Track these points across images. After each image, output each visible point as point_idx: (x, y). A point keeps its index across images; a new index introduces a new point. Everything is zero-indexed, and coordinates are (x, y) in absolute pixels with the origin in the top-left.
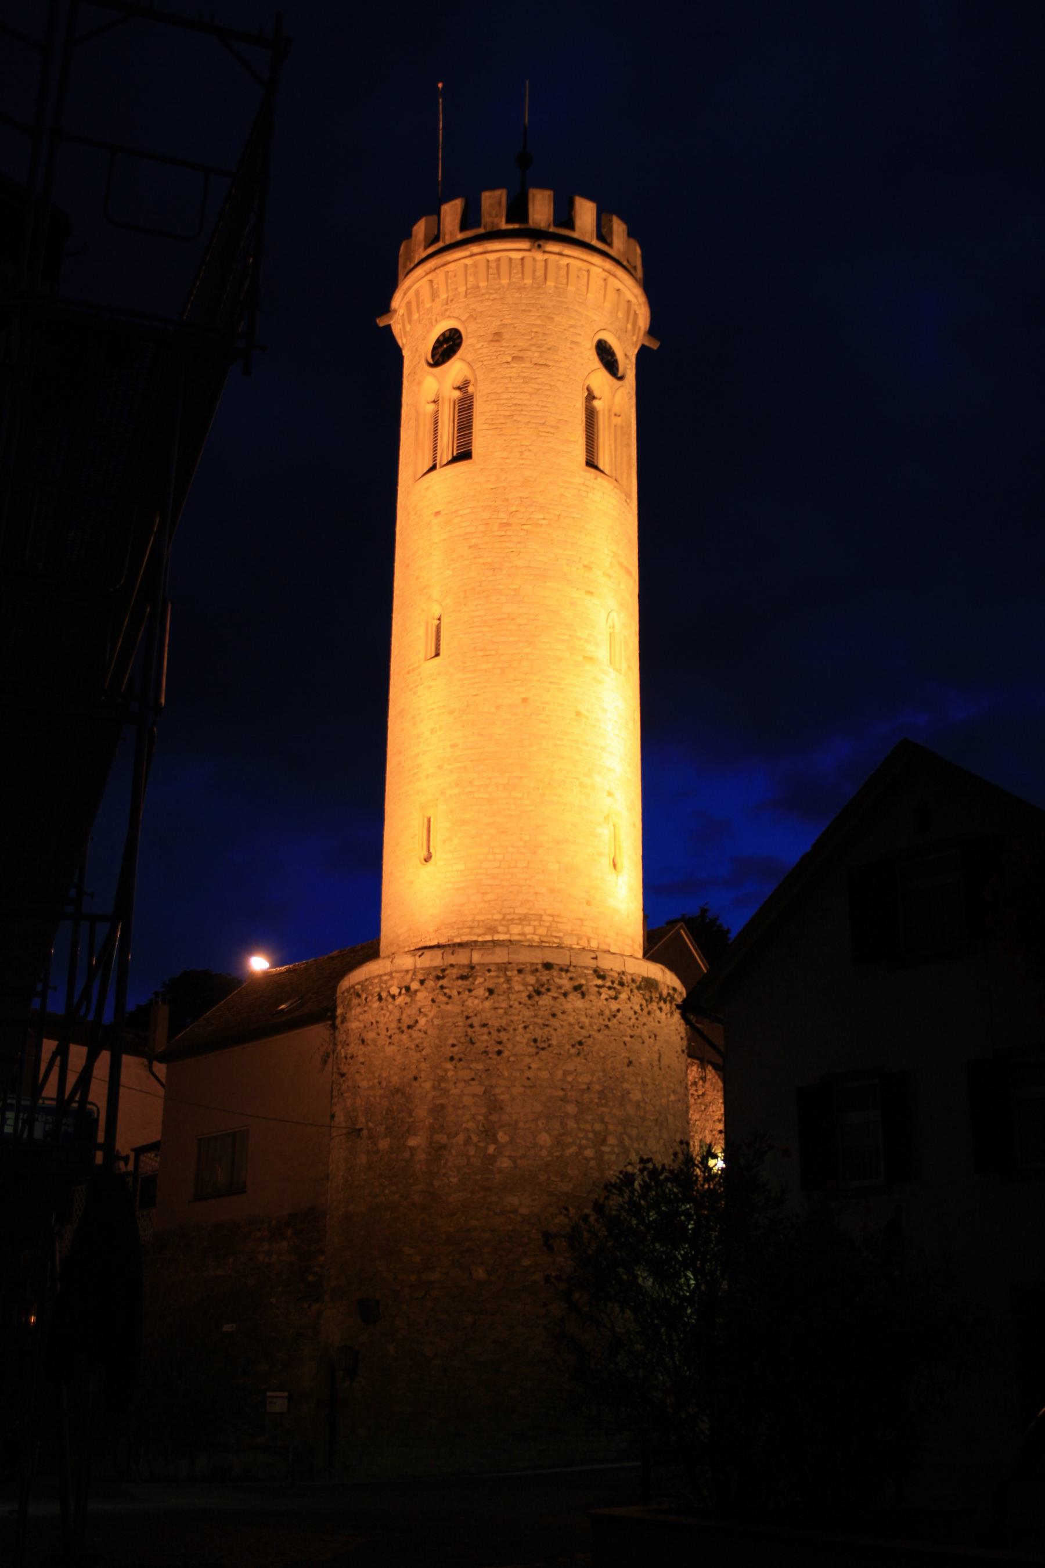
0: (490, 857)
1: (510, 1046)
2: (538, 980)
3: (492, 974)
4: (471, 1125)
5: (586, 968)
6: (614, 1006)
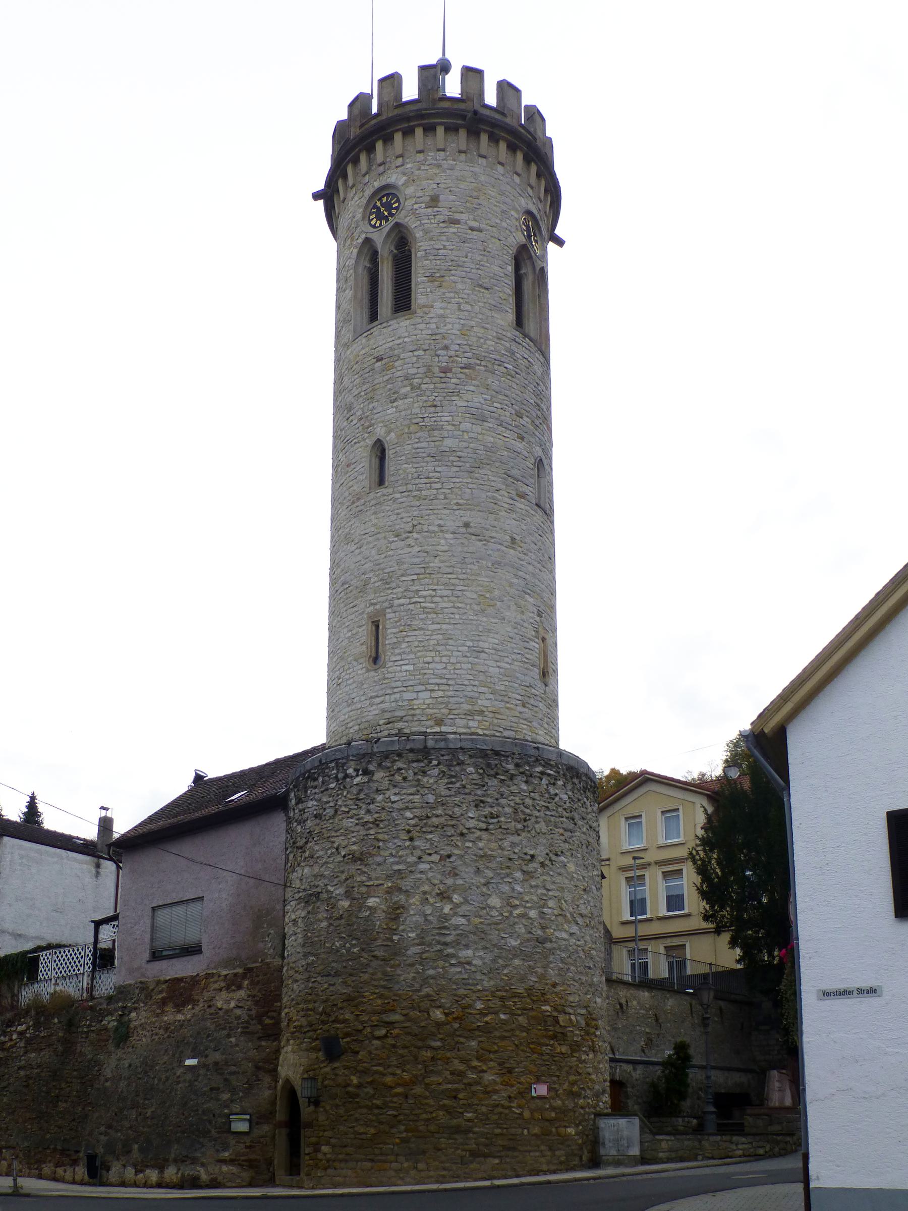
3: (445, 758)
5: (530, 756)
6: (552, 790)
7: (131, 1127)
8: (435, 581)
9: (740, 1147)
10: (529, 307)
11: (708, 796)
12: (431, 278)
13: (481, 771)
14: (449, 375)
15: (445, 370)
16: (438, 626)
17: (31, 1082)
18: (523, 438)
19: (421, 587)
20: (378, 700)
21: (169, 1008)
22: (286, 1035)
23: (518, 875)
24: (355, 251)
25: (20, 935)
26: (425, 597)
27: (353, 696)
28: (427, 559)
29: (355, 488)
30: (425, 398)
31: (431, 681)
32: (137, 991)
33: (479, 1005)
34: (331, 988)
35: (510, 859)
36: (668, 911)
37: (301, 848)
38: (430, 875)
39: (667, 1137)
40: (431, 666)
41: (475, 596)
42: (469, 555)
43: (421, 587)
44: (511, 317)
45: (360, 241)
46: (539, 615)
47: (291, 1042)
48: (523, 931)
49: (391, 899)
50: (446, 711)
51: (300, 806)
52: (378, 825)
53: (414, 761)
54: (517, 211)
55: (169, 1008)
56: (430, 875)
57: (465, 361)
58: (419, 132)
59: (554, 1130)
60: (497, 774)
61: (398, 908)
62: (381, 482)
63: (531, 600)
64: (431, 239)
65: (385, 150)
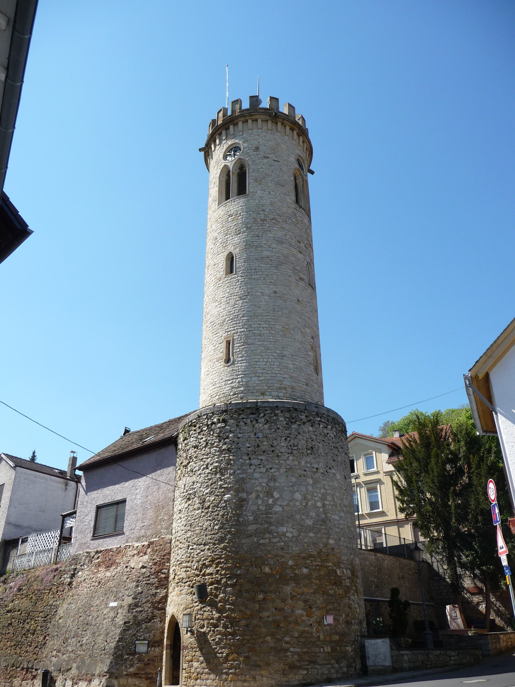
0: (261, 360)
1: (278, 447)
2: (291, 416)
3: (268, 412)
4: (259, 488)
5: (313, 412)
6: (326, 431)
7: (72, 651)
8: (260, 320)
9: (452, 658)
10: (300, 195)
11: (388, 445)
12: (256, 180)
13: (288, 419)
14: (265, 223)
15: (263, 220)
16: (262, 343)
17: (13, 620)
18: (301, 253)
19: (253, 323)
20: (229, 382)
21: (102, 569)
22: (172, 586)
23: (311, 481)
24: (220, 170)
25: (18, 526)
26: (254, 328)
27: (215, 380)
28: (255, 309)
29: (218, 275)
30: (254, 233)
31: (258, 372)
32: (84, 558)
33: (290, 563)
34: (202, 553)
35: (305, 471)
36: (371, 510)
37: (186, 466)
38: (260, 480)
39: (407, 652)
40: (258, 363)
41: (280, 327)
42: (277, 307)
43: (253, 323)
44: (294, 198)
45: (222, 166)
46: (312, 338)
47: (176, 589)
48: (314, 515)
49: (238, 495)
50: (266, 388)
51: (186, 442)
52: (230, 451)
53: (250, 414)
54: (294, 155)
55: (102, 569)
56: (260, 480)
57: (273, 216)
58: (250, 121)
59: (338, 648)
60: (296, 421)
61: (242, 501)
62: (231, 272)
63: (308, 330)
64: (256, 164)
65: (234, 130)
